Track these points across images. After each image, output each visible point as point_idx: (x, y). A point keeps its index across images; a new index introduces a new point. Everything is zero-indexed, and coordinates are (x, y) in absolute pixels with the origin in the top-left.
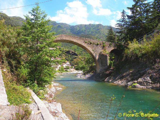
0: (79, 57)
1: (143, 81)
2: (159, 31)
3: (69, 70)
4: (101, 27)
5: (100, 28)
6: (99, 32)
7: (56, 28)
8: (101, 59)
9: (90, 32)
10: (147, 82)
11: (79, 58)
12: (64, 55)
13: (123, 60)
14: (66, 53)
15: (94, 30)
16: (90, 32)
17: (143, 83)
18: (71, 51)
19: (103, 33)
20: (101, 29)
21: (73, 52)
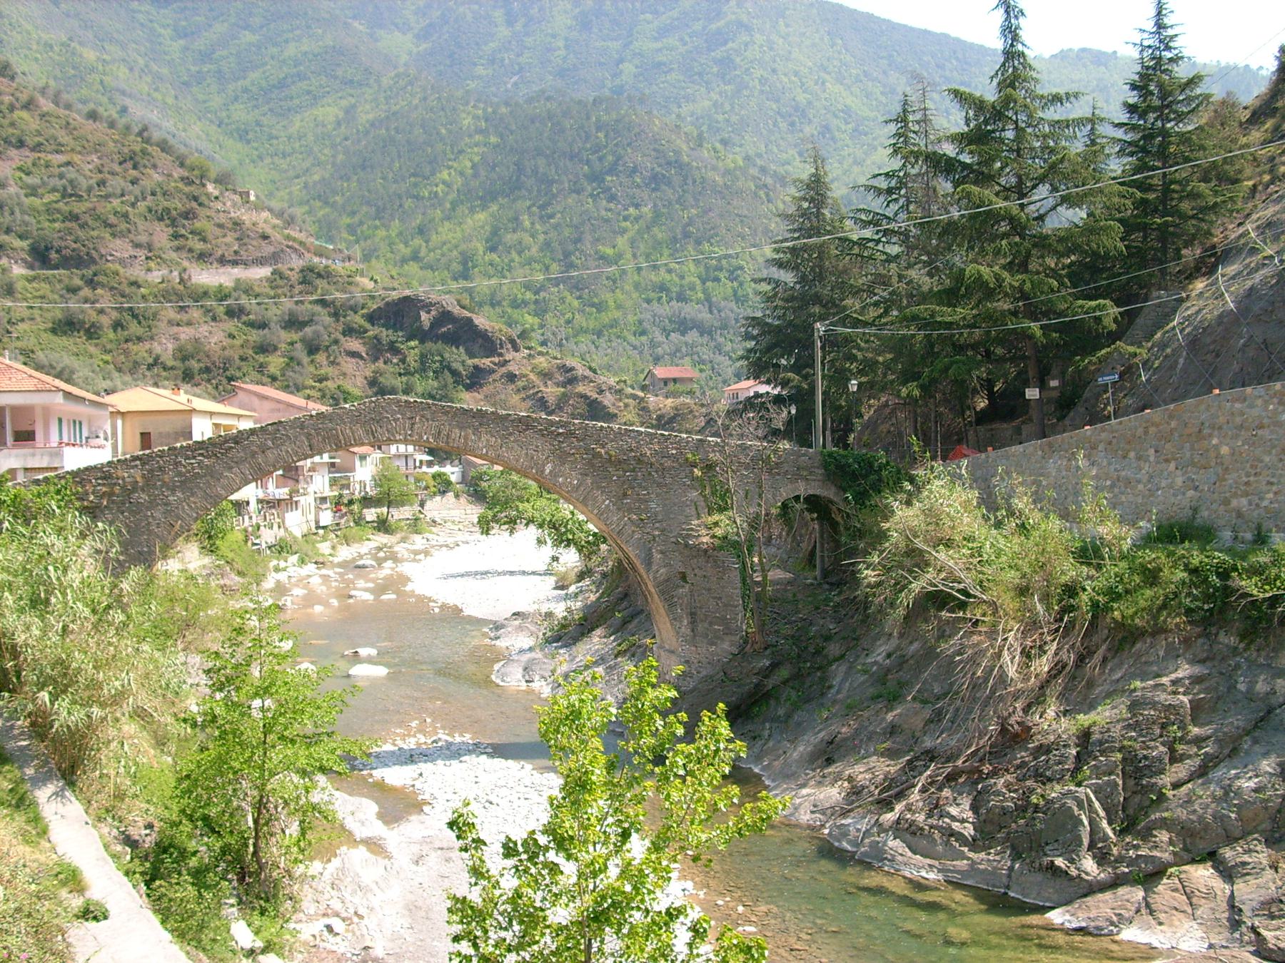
0: (512, 367)
1: (931, 827)
2: (1058, 420)
3: (400, 514)
4: (744, 18)
5: (740, 24)
6: (726, 63)
7: (257, 21)
8: (690, 577)
9: (629, 68)
10: (952, 833)
11: (511, 377)
12: (355, 345)
13: (1073, 258)
14: (371, 318)
15: (672, 41)
16: (629, 68)
17: (930, 835)
18: (428, 306)
19: (763, 81)
20: (748, 29)
21: (445, 316)
